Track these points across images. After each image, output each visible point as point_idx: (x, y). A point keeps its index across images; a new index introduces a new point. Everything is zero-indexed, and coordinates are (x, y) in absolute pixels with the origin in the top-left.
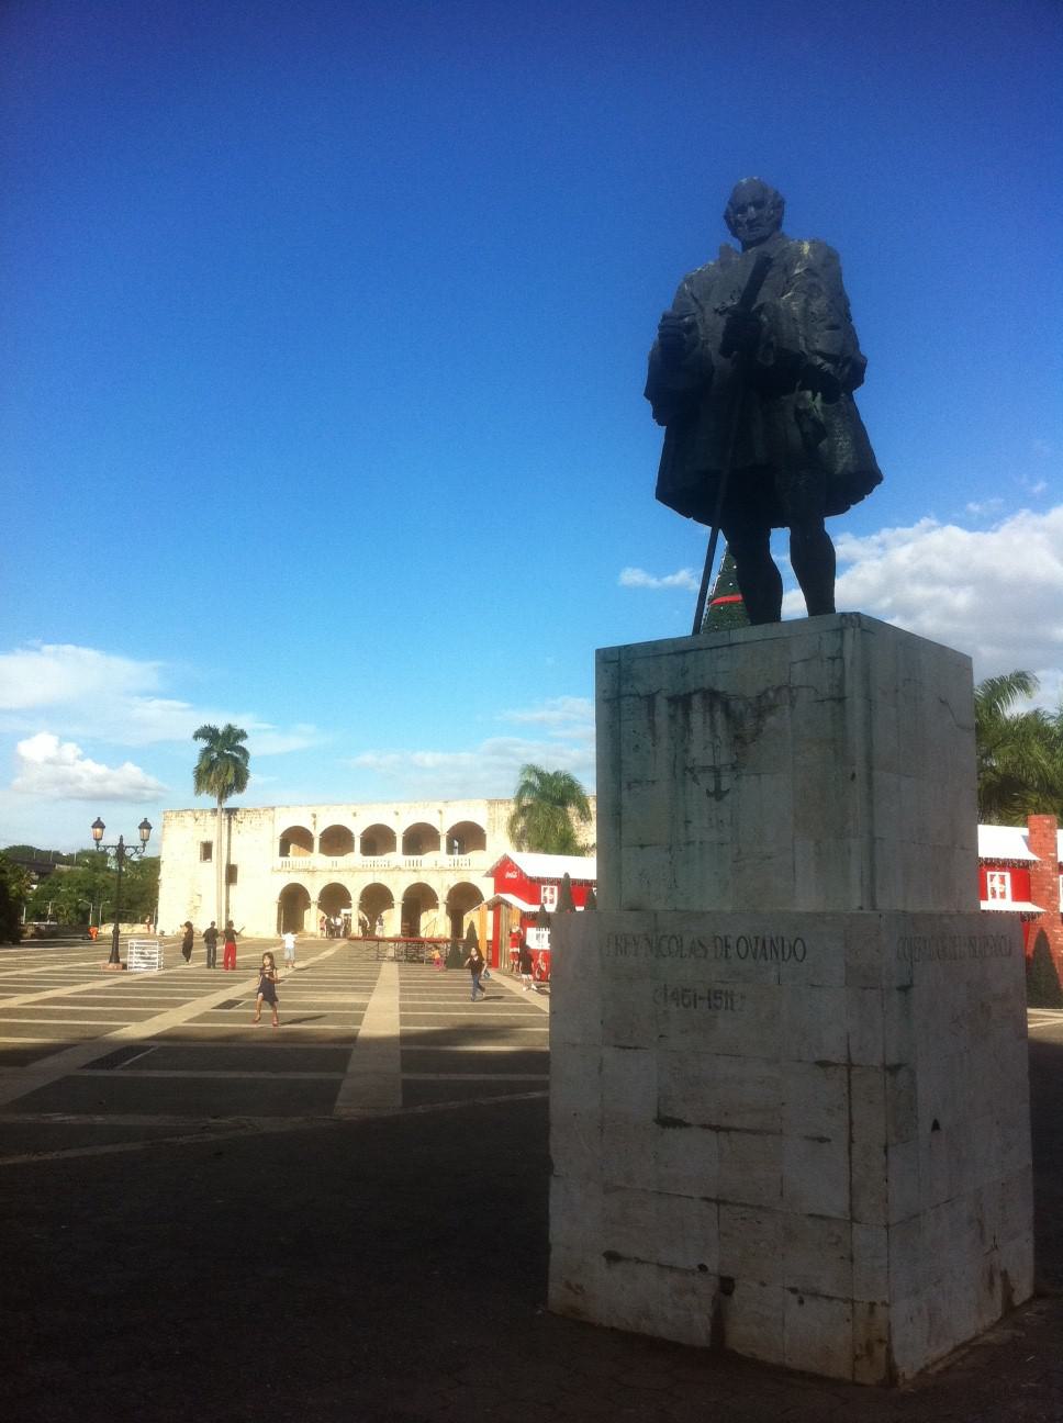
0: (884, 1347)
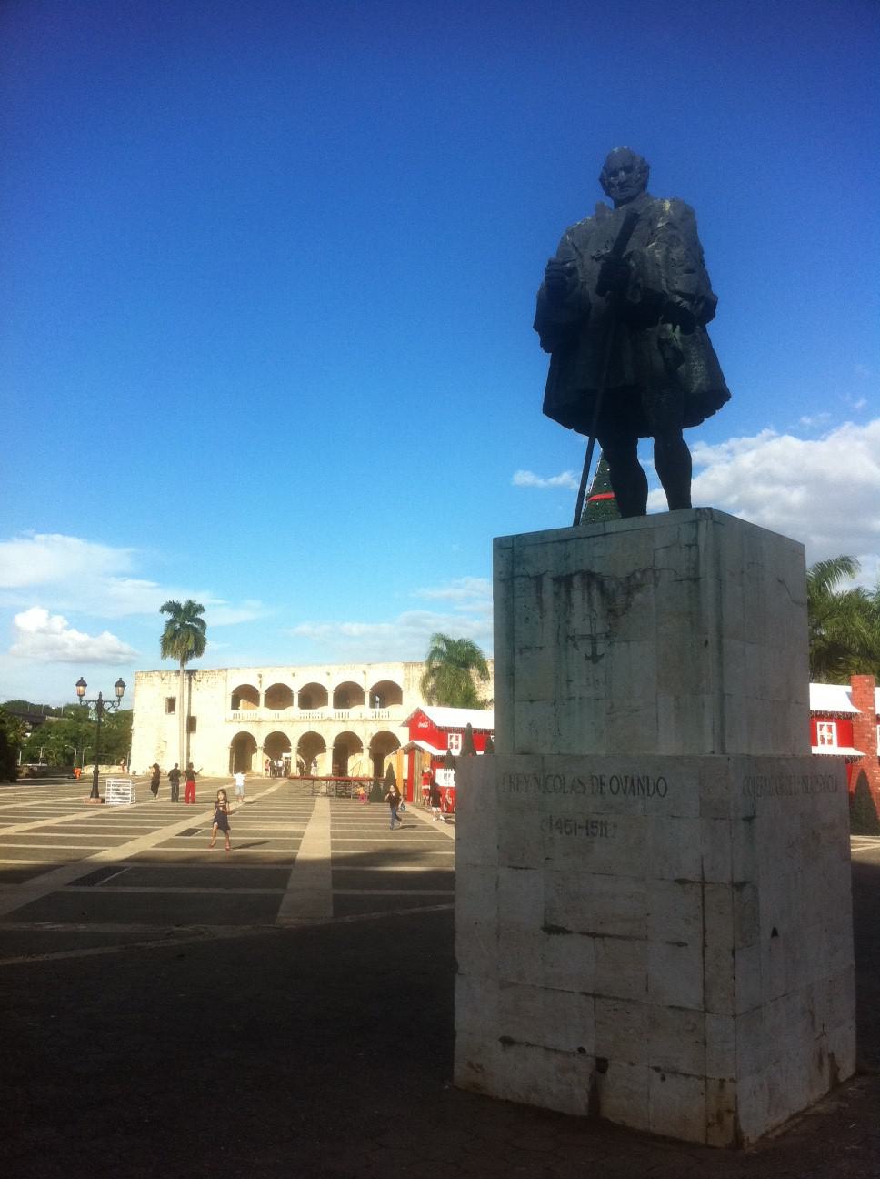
0: (732, 1116)
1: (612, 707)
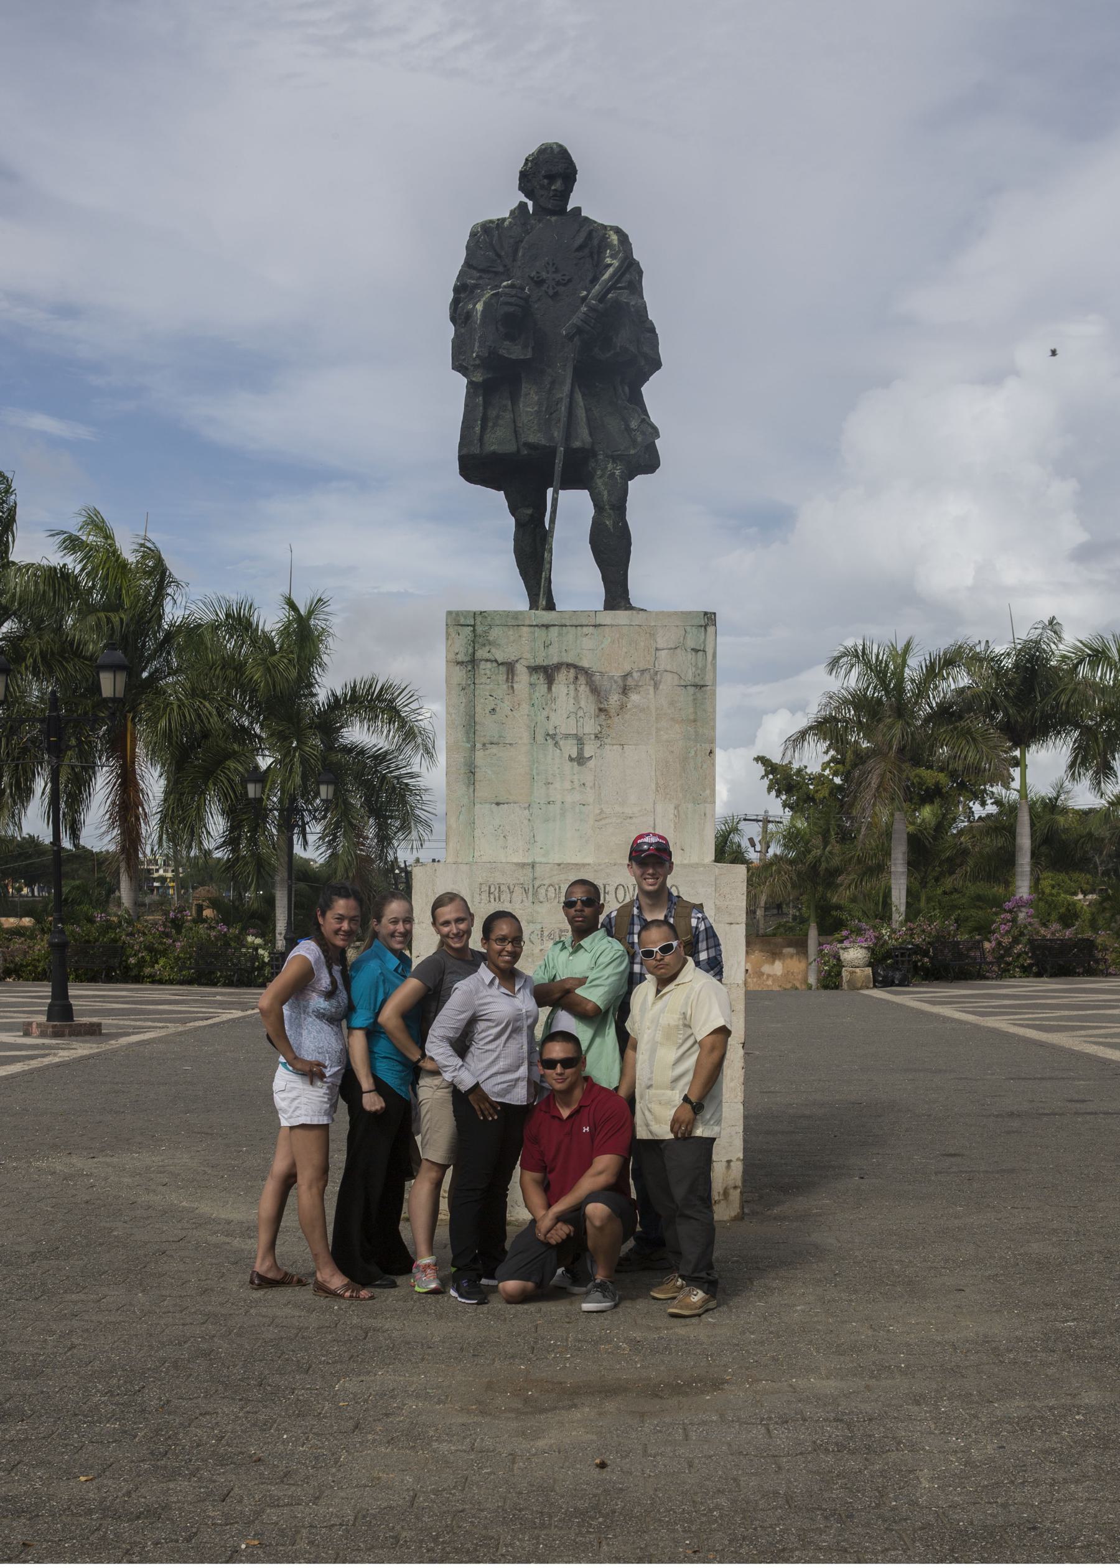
1: (602, 812)
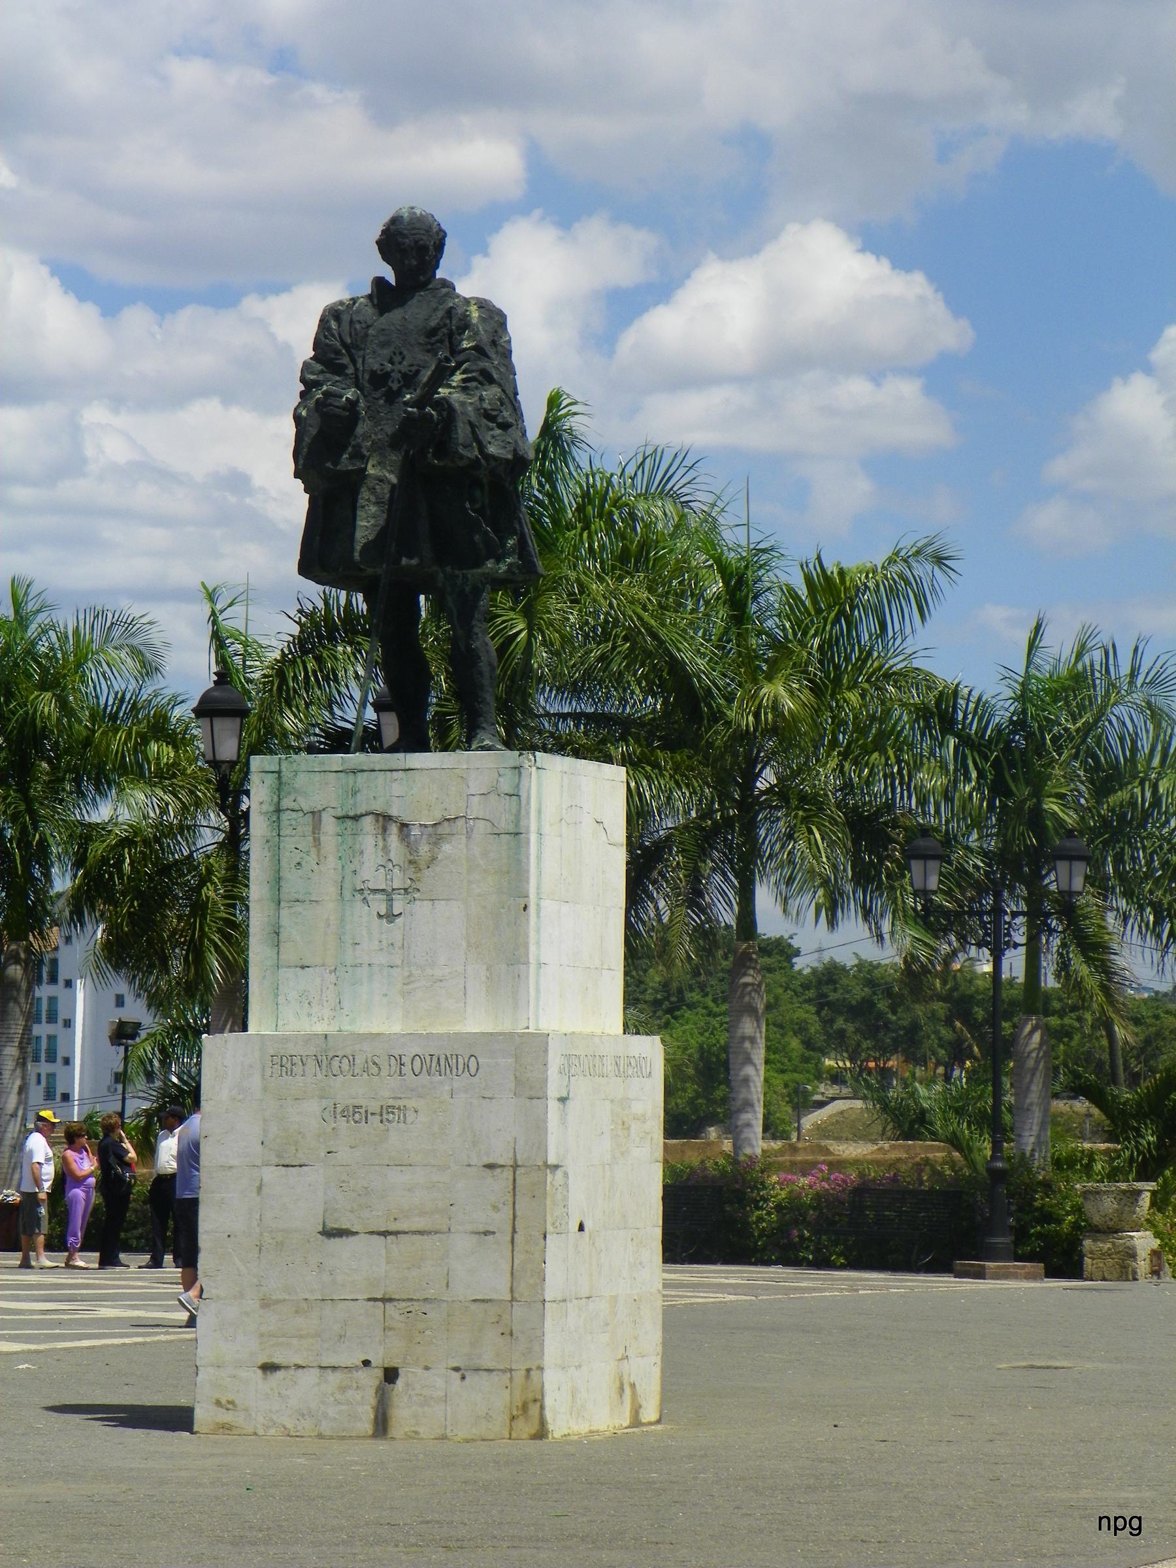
0: (538, 1404)
